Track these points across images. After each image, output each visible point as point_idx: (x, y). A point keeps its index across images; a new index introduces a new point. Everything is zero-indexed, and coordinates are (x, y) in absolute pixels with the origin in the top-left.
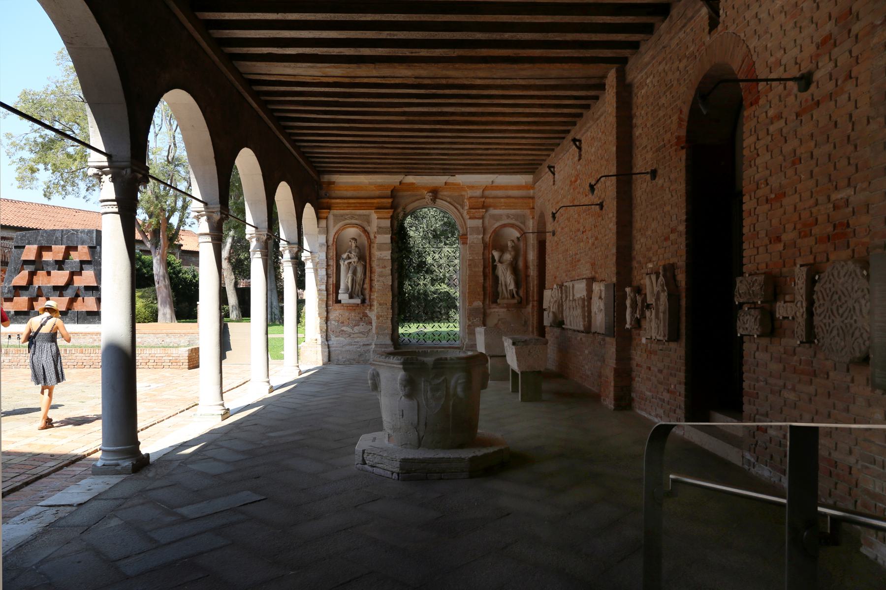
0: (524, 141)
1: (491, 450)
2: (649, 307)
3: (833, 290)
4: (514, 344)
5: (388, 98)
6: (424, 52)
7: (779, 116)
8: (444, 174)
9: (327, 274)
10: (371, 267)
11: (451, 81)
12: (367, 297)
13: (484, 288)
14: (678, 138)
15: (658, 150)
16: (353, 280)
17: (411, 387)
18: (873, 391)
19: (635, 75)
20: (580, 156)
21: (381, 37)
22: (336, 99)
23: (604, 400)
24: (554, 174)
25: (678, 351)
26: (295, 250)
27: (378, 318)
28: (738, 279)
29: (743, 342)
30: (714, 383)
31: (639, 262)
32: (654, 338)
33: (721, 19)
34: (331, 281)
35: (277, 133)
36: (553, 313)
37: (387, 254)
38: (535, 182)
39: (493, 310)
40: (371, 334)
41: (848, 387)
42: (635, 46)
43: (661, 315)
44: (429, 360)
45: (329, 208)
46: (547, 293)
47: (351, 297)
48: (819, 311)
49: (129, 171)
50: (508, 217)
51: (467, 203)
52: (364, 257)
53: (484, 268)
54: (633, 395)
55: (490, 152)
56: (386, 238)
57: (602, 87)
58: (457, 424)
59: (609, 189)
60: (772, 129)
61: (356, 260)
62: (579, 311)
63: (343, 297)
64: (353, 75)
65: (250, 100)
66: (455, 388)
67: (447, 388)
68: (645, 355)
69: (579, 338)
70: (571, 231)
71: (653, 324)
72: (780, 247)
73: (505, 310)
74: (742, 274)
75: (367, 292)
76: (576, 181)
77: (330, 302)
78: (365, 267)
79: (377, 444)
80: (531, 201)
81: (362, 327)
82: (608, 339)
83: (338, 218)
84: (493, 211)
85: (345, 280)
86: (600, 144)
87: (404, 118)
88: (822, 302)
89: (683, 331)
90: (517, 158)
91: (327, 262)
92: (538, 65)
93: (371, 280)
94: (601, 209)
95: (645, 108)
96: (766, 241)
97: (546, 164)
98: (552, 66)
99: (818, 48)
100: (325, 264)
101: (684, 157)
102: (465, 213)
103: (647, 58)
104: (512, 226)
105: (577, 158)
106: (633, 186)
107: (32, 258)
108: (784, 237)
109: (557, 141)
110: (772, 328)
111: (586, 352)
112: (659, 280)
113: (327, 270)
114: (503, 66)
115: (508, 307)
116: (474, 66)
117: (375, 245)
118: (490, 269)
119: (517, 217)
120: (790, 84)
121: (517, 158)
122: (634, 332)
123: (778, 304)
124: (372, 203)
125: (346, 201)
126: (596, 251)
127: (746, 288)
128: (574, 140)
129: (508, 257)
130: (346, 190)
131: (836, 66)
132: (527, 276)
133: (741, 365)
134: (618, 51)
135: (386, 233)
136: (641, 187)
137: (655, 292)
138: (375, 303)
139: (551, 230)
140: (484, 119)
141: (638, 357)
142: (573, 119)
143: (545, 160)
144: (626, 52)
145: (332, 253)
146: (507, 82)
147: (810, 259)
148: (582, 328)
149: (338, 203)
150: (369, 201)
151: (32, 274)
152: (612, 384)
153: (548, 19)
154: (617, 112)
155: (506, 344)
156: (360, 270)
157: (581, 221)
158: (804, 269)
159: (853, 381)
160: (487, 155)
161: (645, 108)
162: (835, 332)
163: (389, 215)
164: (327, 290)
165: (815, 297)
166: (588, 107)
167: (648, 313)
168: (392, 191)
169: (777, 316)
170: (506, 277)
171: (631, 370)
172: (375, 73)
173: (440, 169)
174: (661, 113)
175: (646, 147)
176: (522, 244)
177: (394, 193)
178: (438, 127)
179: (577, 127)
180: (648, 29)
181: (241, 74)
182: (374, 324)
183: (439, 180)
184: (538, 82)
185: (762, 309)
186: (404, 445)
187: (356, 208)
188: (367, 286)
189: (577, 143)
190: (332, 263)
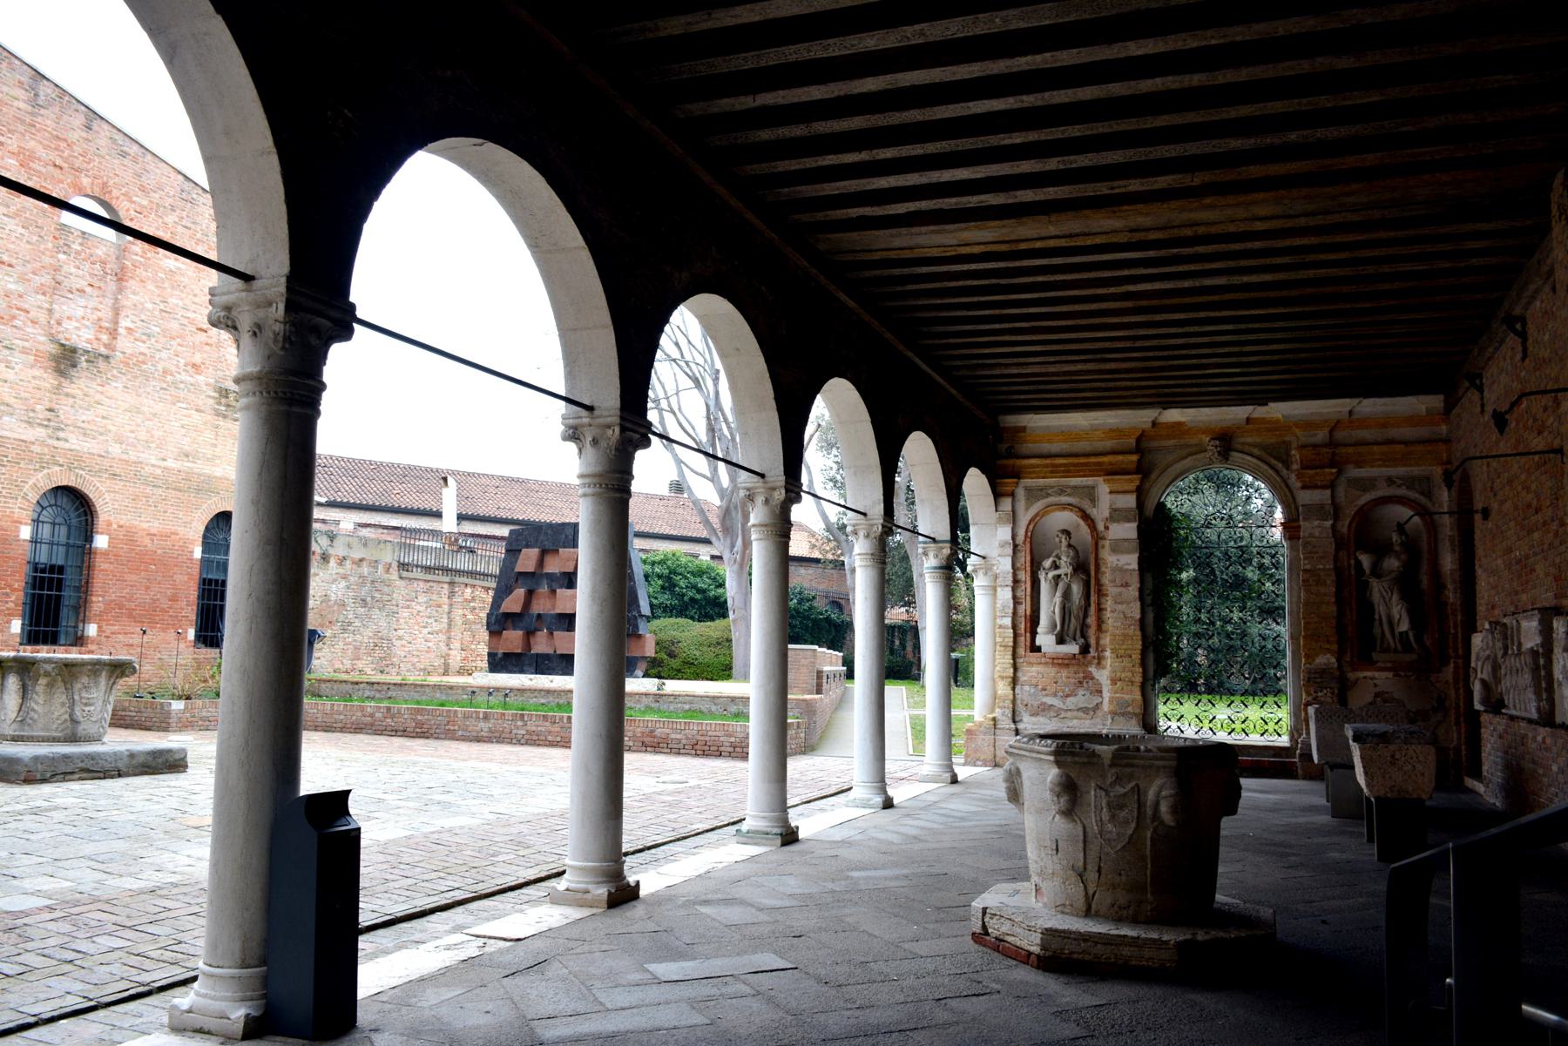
5: (1078, 271)
6: (1134, 185)
9: (1014, 597)
10: (1099, 584)
11: (1201, 230)
12: (1092, 641)
16: (1063, 608)
17: (1070, 792)
20: (1525, 351)
21: (1048, 168)
22: (994, 281)
26: (947, 551)
27: (1114, 681)
34: (1021, 609)
36: (1483, 681)
37: (1131, 561)
39: (1361, 674)
40: (1099, 713)
45: (1017, 475)
46: (1477, 640)
50: (1390, 481)
52: (1086, 568)
56: (1128, 530)
61: (1069, 570)
63: (1045, 639)
64: (1013, 237)
69: (1539, 738)
73: (1390, 675)
75: (1092, 632)
77: (1021, 651)
78: (1087, 585)
80: (1442, 446)
81: (1082, 699)
83: (1033, 495)
84: (1354, 472)
85: (1049, 607)
87: (1129, 304)
91: (1015, 575)
93: (1100, 610)
100: (1010, 578)
104: (1401, 501)
105: (1519, 356)
107: (531, 569)
111: (1555, 768)
113: (1014, 590)
115: (1395, 669)
117: (1107, 543)
119: (1410, 482)
124: (1099, 464)
125: (1048, 461)
129: (1392, 563)
130: (1049, 441)
138: (1108, 654)
145: (1025, 558)
148: (1535, 715)
149: (1033, 466)
150: (1093, 460)
151: (530, 594)
156: (1076, 589)
157: (1533, 486)
163: (1133, 486)
164: (1014, 627)
168: (1138, 440)
170: (1393, 612)
172: (1052, 230)
182: (1106, 695)
186: (1061, 909)
187: (1068, 472)
188: (1091, 620)
189: (1518, 326)
190: (1024, 576)
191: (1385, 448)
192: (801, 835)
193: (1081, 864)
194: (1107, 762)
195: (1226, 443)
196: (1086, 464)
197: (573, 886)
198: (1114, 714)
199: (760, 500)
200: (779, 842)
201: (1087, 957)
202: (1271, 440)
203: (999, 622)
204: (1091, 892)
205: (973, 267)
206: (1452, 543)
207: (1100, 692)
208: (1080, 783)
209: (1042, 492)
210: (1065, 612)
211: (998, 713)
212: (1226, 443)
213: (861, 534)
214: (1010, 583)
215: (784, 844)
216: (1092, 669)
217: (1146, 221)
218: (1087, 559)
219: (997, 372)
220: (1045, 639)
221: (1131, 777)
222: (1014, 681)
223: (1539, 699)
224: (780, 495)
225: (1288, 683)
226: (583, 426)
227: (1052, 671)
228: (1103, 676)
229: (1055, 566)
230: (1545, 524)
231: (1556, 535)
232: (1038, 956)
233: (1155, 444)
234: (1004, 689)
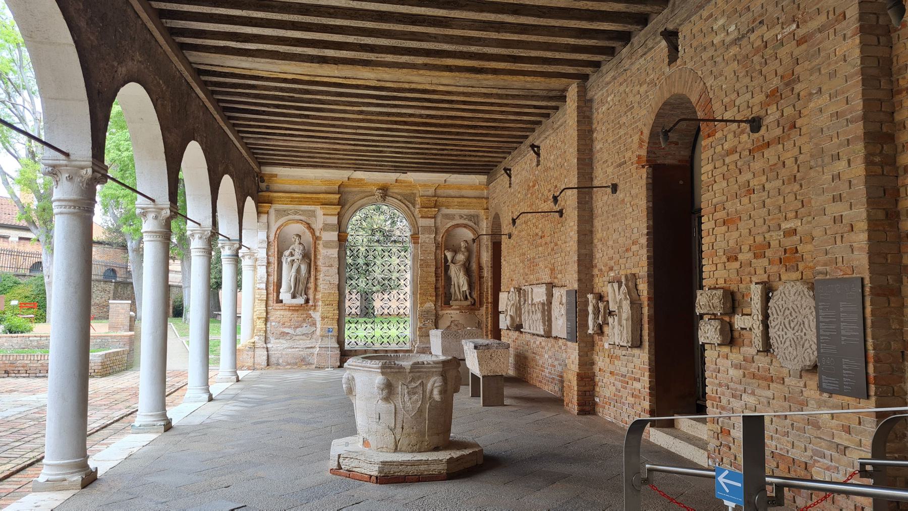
0: (481, 144)
1: (467, 452)
2: (611, 313)
3: (785, 306)
4: (476, 347)
7: (733, 151)
8: (395, 171)
9: (267, 272)
11: (413, 86)
12: (311, 297)
13: (436, 288)
14: (639, 157)
15: (620, 165)
18: (821, 395)
19: (596, 93)
23: (567, 405)
24: (510, 177)
25: (642, 358)
27: (323, 318)
28: (699, 292)
29: (705, 350)
30: (678, 385)
31: (601, 270)
32: (617, 343)
33: (680, 54)
34: (271, 278)
35: (222, 124)
38: (489, 183)
39: (445, 312)
40: (314, 336)
41: (802, 392)
42: (597, 65)
43: (624, 322)
44: (407, 364)
45: (270, 202)
46: (503, 296)
47: (294, 297)
48: (773, 324)
49: (90, 171)
50: (461, 217)
51: (418, 200)
52: (309, 257)
53: (436, 268)
54: (597, 400)
55: (445, 152)
57: (563, 98)
58: (437, 427)
59: (570, 200)
60: (727, 160)
62: (539, 315)
63: (285, 296)
65: (198, 90)
66: (432, 390)
67: (424, 391)
68: (608, 360)
69: (538, 343)
70: (529, 235)
71: (616, 331)
72: (736, 265)
74: (701, 287)
75: (311, 292)
76: (534, 186)
77: (271, 303)
79: (350, 448)
80: (485, 201)
81: (306, 329)
82: (569, 343)
83: (280, 213)
84: (445, 211)
86: (559, 153)
87: (361, 117)
88: (775, 316)
89: (646, 338)
90: (473, 159)
91: (268, 259)
92: (502, 77)
93: (316, 279)
94: (561, 216)
95: (606, 124)
96: (724, 259)
97: (503, 165)
98: (515, 78)
99: (767, 97)
101: (645, 176)
102: (417, 212)
103: (608, 79)
104: (465, 226)
105: (535, 164)
106: (594, 197)
108: (740, 257)
109: (515, 145)
110: (730, 338)
112: (622, 289)
114: (467, 75)
116: (437, 73)
118: (443, 269)
119: (471, 217)
120: (743, 125)
121: (473, 159)
122: (596, 337)
123: (736, 316)
124: (318, 198)
126: (556, 256)
127: (704, 301)
128: (533, 146)
129: (461, 257)
131: (783, 115)
132: (481, 277)
133: (703, 371)
134: (580, 68)
135: (333, 231)
136: (602, 200)
137: (618, 300)
138: (320, 303)
139: (506, 232)
140: (443, 122)
141: (601, 362)
142: (532, 126)
143: (501, 162)
144: (588, 70)
145: (274, 249)
146: (470, 90)
147: (765, 278)
148: (542, 333)
149: (278, 197)
150: (314, 196)
152: (576, 388)
153: (515, 37)
154: (578, 126)
155: (465, 348)
156: (304, 268)
157: (540, 226)
158: (760, 287)
159: (805, 386)
160: (442, 155)
161: (606, 124)
162: (788, 343)
163: (336, 212)
164: (267, 289)
165: (769, 311)
166: (547, 116)
167: (610, 320)
168: (339, 187)
169: (736, 327)
170: (459, 280)
171: (594, 375)
172: (337, 73)
173: (392, 166)
174: (622, 132)
175: (607, 161)
176: (475, 247)
177: (341, 190)
178: (395, 126)
179: (536, 134)
180: (611, 52)
181: (191, 63)
182: (319, 325)
183: (389, 177)
184: (499, 92)
185: (722, 320)
186: (380, 449)
187: (300, 202)
188: (311, 285)
190: (274, 260)
191: (459, 200)
192: (173, 424)
193: (393, 425)
194: (408, 371)
195: (385, 192)
196: (311, 198)
197: (51, 478)
198: (322, 336)
199: (151, 216)
200: (163, 429)
201: (402, 474)
202: (407, 191)
203: (258, 286)
204: (398, 439)
205: (283, 85)
206: (487, 247)
207: (314, 324)
208: (393, 382)
209: (285, 213)
210: (297, 280)
211: (256, 339)
212: (385, 192)
213: (197, 236)
214: (265, 264)
215: (165, 431)
216: (311, 312)
217: (386, 76)
218: (309, 251)
219: (271, 143)
220: (285, 296)
221: (419, 378)
222: (266, 320)
223: (544, 324)
224: (167, 213)
225: (646, 344)
226: (61, 166)
227: (288, 313)
228: (317, 316)
229: (292, 255)
230: (546, 243)
231: (553, 250)
232: (377, 477)
233: (348, 189)
234: (260, 324)
